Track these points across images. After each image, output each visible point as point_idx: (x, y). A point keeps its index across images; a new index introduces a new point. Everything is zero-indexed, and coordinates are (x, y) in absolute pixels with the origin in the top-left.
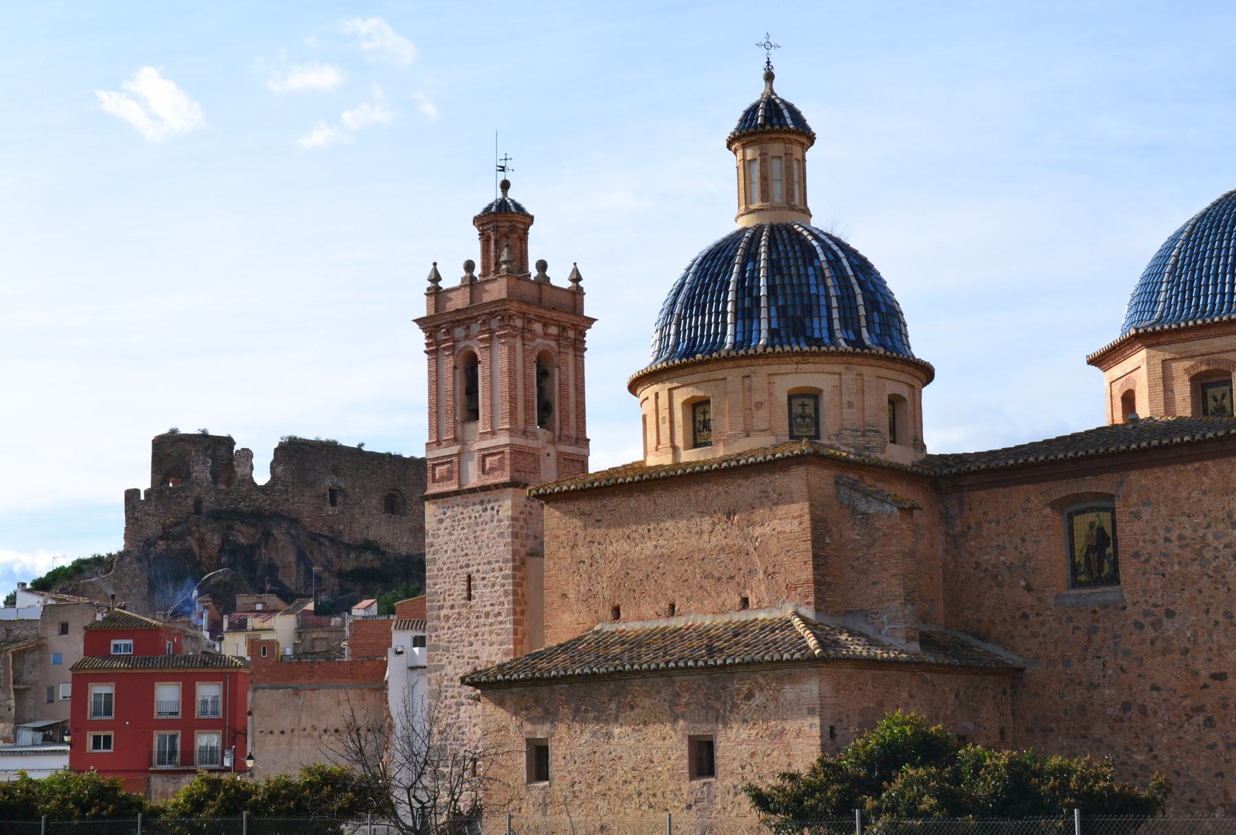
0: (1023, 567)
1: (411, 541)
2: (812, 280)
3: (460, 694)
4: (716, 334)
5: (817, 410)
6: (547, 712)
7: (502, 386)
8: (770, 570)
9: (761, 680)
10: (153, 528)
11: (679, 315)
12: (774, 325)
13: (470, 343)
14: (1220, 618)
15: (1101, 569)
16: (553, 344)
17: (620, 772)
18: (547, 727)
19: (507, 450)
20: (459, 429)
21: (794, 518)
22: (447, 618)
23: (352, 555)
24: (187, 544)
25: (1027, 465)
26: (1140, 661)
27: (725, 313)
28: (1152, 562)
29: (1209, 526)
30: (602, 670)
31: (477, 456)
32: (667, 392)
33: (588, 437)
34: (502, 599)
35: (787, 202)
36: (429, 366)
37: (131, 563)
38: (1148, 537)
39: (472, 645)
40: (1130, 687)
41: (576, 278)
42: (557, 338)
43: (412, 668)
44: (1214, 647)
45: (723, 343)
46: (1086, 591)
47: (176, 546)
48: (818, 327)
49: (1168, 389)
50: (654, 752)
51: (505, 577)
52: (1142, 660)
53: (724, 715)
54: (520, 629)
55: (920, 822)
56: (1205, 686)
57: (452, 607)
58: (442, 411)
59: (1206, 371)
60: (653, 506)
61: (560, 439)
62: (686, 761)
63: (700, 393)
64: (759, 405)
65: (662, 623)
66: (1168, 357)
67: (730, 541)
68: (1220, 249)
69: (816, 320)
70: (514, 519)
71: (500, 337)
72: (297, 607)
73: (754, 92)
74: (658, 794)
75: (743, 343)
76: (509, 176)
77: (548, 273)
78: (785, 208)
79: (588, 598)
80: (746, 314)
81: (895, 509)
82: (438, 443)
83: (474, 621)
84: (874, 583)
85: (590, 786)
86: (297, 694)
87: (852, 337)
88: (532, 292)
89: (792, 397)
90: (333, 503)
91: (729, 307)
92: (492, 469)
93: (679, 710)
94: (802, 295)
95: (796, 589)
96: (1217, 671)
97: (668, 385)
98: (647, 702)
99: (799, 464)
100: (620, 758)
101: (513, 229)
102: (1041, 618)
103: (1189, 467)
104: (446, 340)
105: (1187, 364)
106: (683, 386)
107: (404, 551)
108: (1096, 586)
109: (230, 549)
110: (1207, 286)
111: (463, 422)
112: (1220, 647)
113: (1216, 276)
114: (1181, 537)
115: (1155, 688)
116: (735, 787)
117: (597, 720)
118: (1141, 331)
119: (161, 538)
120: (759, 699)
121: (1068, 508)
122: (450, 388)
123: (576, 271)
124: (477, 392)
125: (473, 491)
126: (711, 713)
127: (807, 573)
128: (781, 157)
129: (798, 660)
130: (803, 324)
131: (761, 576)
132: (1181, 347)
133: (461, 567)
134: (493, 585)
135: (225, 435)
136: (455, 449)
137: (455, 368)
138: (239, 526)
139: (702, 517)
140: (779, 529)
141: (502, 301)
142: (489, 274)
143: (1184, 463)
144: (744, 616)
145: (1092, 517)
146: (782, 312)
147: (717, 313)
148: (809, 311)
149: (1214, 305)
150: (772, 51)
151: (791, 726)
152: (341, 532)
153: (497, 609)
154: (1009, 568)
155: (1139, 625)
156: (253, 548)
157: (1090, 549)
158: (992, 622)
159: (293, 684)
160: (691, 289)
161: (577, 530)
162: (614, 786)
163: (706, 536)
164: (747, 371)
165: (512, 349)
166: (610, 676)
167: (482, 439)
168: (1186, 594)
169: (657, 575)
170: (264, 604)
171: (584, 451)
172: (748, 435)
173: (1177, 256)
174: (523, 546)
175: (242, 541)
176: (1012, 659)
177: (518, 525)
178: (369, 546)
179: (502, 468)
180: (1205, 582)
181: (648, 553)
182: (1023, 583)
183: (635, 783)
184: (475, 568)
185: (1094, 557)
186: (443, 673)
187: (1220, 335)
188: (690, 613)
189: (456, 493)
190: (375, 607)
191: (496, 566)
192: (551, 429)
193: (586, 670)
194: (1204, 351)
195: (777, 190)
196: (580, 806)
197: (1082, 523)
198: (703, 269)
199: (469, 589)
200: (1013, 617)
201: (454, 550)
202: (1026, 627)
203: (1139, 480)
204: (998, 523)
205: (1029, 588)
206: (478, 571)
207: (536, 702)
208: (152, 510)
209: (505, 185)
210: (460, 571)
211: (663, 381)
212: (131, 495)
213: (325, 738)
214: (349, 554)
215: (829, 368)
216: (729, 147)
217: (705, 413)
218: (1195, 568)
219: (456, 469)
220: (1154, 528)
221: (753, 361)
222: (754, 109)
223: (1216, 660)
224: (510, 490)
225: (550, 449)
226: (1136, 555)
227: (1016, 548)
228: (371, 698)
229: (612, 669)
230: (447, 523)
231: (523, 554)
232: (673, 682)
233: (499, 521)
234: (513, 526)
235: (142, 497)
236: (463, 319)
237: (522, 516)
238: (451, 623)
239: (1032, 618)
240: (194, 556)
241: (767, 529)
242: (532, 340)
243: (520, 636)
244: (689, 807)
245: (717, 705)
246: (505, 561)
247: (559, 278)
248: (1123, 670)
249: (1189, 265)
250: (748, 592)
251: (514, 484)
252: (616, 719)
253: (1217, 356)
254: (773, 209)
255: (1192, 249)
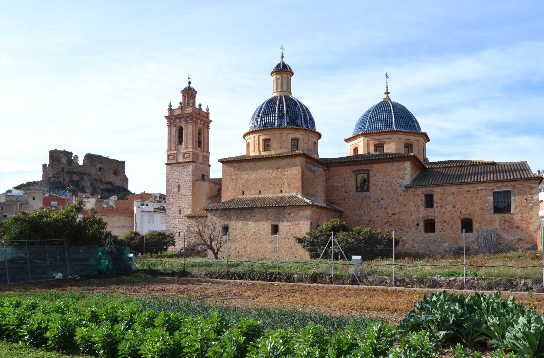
0: (345, 187)
1: (120, 182)
2: (297, 110)
3: (175, 216)
4: (272, 122)
5: (297, 144)
6: (228, 217)
7: (190, 136)
8: (289, 183)
9: (293, 210)
10: (50, 174)
11: (261, 117)
12: (288, 121)
13: (181, 124)
14: (395, 201)
15: (364, 188)
16: (202, 126)
17: (250, 233)
18: (228, 222)
19: (191, 153)
20: (177, 146)
21: (297, 170)
22: (172, 196)
23: (105, 185)
24: (60, 180)
25: (348, 161)
26: (374, 210)
27: (275, 117)
28: (379, 186)
29: (394, 178)
30: (247, 207)
31: (182, 154)
32: (258, 136)
33: (210, 151)
34: (189, 192)
35: (287, 90)
36: (168, 129)
37: (44, 183)
38: (378, 180)
39: (179, 203)
40: (371, 217)
41: (208, 110)
42: (203, 125)
43: (142, 211)
44: (393, 207)
45: (274, 124)
46: (361, 193)
47: (57, 180)
48: (299, 123)
49: (368, 147)
50: (261, 228)
51: (190, 186)
52: (374, 210)
53: (282, 219)
54: (193, 199)
55: (351, 245)
56: (390, 217)
57: (174, 193)
58: (172, 142)
59: (378, 144)
60: (255, 166)
61: (203, 151)
62: (270, 231)
63: (267, 137)
64: (284, 141)
65: (257, 196)
66: (369, 139)
67: (278, 175)
68: (382, 114)
69: (298, 120)
70: (193, 171)
71: (190, 123)
72: (96, 197)
73: (278, 61)
74: (262, 239)
75: (280, 124)
76: (191, 80)
77: (202, 107)
78: (286, 91)
79: (235, 189)
80: (281, 117)
81: (322, 169)
82: (170, 150)
83: (180, 197)
84: (316, 188)
85: (241, 237)
86: (108, 217)
87: (307, 126)
88: (198, 112)
89: (292, 140)
90: (100, 171)
91: (276, 115)
92: (187, 158)
93: (268, 217)
94: (295, 114)
95: (296, 188)
96: (394, 213)
97: (258, 135)
98: (259, 215)
99: (299, 156)
100: (250, 230)
101: (192, 95)
102: (348, 199)
103: (389, 164)
104: (173, 123)
105: (373, 141)
106: (263, 135)
107: (118, 185)
108: (362, 192)
109: (72, 182)
110: (379, 123)
111: (178, 145)
112: (395, 207)
113: (381, 121)
114: (386, 181)
115: (377, 217)
116: (284, 237)
117: (244, 220)
118: (363, 133)
119: (53, 177)
120: (292, 215)
121: (357, 173)
122: (174, 135)
123: (208, 108)
124: (182, 137)
125: (181, 163)
126: (278, 218)
127: (300, 184)
128: (286, 78)
129: (306, 205)
130: (295, 121)
131: (286, 184)
132: (372, 137)
133: (177, 183)
134: (186, 188)
135: (70, 151)
136: (175, 152)
137: (176, 130)
138: (74, 175)
139: (270, 169)
140: (292, 173)
141: (191, 113)
142: (185, 106)
143: (388, 163)
144: (281, 195)
145: (362, 175)
146: (290, 117)
147: (273, 117)
148: (297, 118)
149: (381, 128)
150: (283, 50)
151: (301, 222)
152: (102, 179)
153: (187, 194)
154: (341, 187)
155: (374, 202)
156: (78, 182)
157: (361, 183)
158: (336, 200)
159: (107, 214)
160: (264, 110)
161: (232, 171)
162: (248, 237)
163: (271, 174)
164: (281, 132)
165: (193, 126)
166: (249, 208)
167: (184, 149)
168: (387, 194)
169: (256, 184)
170: (86, 195)
171: (208, 155)
172: (281, 149)
173: (371, 115)
174: (195, 178)
175: (76, 180)
176: (341, 209)
177: (193, 173)
178: (110, 183)
179: (189, 157)
180: (392, 192)
181: (253, 178)
182: (344, 191)
183: (255, 236)
184: (181, 183)
185: (362, 185)
186: (171, 210)
187: (382, 135)
188: (265, 194)
189: (176, 163)
190: (116, 198)
191: (187, 183)
192: (201, 149)
193: (242, 207)
194: (378, 139)
195: (285, 87)
196: (238, 242)
197: (360, 177)
198: (267, 105)
199: (179, 189)
200: (341, 199)
201: (175, 178)
202: (344, 201)
203: (376, 166)
204: (338, 175)
205: (346, 192)
206: (182, 184)
207: (225, 215)
208: (50, 170)
209: (190, 83)
210: (176, 184)
211: (256, 134)
212: (44, 166)
213: (116, 229)
214: (104, 184)
215: (302, 133)
216: (271, 75)
217: (268, 142)
218: (389, 188)
219: (176, 157)
220: (380, 178)
221: (283, 130)
222: (279, 65)
223: (393, 210)
224: (192, 163)
225: (201, 154)
226: (375, 185)
227: (343, 182)
228: (129, 219)
229: (250, 206)
230: (173, 171)
231: (194, 180)
232: (267, 210)
233: (188, 171)
234: (192, 173)
235: (48, 166)
236: (179, 117)
237: (194, 170)
238: (173, 197)
239: (346, 199)
240: (62, 183)
241: (289, 173)
242: (198, 124)
243: (193, 201)
244: (271, 242)
245: (280, 216)
246: (190, 182)
247: (204, 109)
248: (369, 212)
249: (374, 118)
250: (283, 189)
251: (193, 162)
252: (250, 219)
253: (381, 140)
254: (284, 91)
255: (375, 114)
